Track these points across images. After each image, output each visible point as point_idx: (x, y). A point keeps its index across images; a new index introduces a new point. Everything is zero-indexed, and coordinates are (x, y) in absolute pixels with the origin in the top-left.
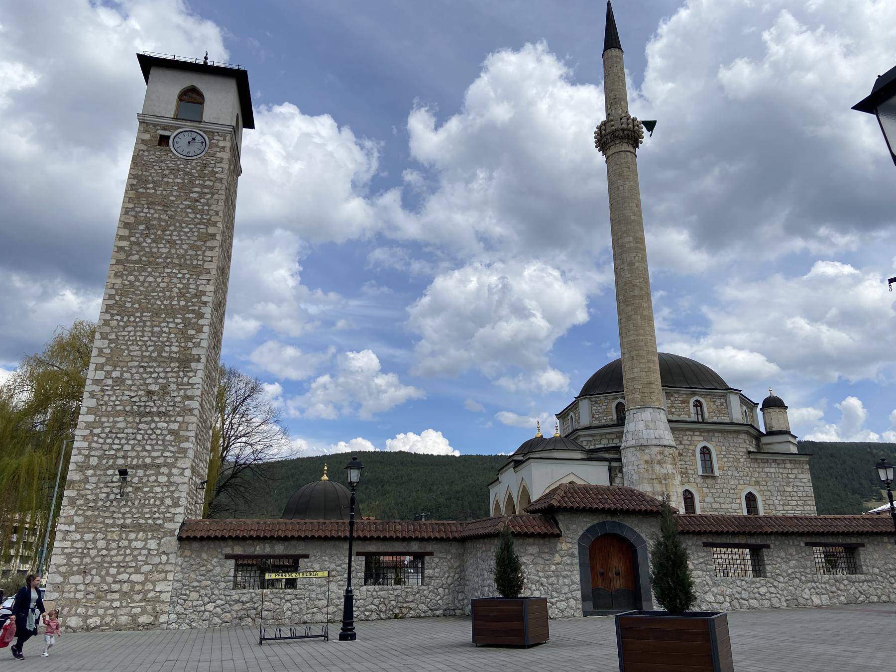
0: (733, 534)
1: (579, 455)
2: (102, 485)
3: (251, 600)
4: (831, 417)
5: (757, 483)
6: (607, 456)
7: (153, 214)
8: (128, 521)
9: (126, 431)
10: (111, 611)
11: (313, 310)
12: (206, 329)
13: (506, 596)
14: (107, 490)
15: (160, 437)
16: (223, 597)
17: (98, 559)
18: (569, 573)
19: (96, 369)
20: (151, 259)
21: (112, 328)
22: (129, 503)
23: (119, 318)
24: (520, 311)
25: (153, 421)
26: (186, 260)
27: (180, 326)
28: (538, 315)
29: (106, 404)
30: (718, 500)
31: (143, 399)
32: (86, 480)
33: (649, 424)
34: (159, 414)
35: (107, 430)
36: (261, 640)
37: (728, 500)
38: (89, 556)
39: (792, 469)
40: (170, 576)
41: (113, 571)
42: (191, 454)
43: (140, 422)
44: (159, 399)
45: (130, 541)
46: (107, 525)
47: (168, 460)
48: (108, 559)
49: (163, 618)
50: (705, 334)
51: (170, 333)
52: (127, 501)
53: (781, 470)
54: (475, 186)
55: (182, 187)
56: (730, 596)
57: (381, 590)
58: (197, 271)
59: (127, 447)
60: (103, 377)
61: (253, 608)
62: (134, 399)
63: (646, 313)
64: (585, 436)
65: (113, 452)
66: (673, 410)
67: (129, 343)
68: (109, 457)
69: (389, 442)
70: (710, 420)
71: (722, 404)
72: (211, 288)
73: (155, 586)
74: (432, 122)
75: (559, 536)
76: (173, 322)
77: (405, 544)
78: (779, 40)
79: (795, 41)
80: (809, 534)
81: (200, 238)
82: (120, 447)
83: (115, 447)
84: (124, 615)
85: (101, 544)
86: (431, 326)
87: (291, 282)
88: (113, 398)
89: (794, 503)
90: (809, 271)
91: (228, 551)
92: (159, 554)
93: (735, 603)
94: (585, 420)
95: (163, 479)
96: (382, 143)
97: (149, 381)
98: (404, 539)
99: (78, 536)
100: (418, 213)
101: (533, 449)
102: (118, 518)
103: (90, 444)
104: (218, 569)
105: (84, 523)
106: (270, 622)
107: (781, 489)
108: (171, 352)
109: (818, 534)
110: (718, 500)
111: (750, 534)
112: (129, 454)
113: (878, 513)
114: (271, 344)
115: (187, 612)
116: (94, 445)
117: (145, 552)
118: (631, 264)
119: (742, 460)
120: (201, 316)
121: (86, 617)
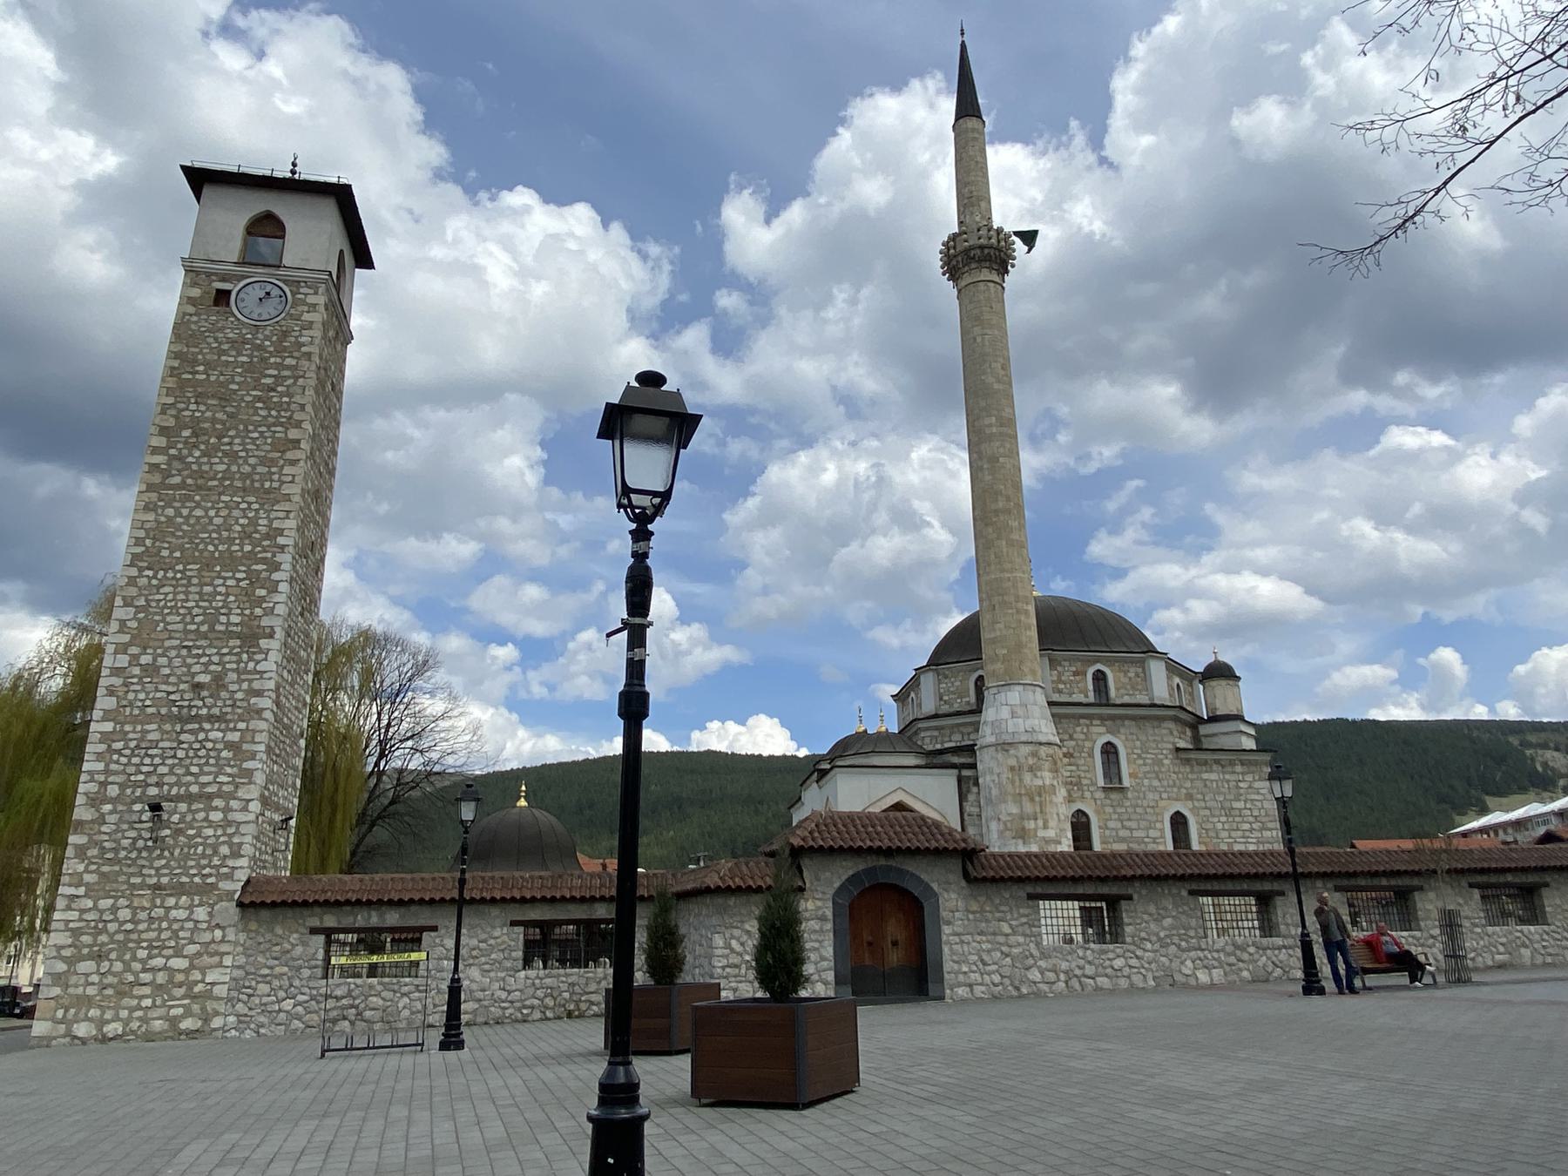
0: (1074, 880)
1: (911, 760)
3: (349, 994)
4: (1410, 679)
5: (1190, 797)
6: (956, 760)
8: (165, 880)
9: (161, 745)
10: (139, 1013)
11: (565, 521)
12: (283, 587)
13: (658, 982)
14: (133, 834)
16: (306, 990)
17: (120, 937)
18: (816, 945)
19: (116, 653)
20: (200, 482)
22: (166, 853)
23: (150, 573)
24: (907, 520)
25: (202, 729)
26: (253, 481)
28: (936, 524)
29: (131, 705)
30: (1127, 824)
31: (186, 696)
32: (101, 820)
33: (1019, 711)
34: (211, 718)
35: (133, 744)
36: (323, 1052)
37: (1143, 824)
38: (107, 931)
40: (228, 961)
41: (142, 954)
42: (260, 778)
43: (182, 731)
44: (211, 696)
47: (225, 788)
48: (134, 936)
49: (217, 1022)
50: (1210, 549)
51: (227, 595)
52: (162, 850)
54: (830, 313)
55: (249, 368)
56: (1066, 972)
57: (547, 976)
58: (270, 497)
59: (163, 770)
61: (352, 1006)
62: (172, 697)
63: (1015, 536)
64: (927, 729)
65: (141, 777)
66: (1061, 686)
68: (136, 785)
69: (696, 735)
70: (1118, 702)
71: (1137, 675)
72: (291, 523)
73: (204, 975)
74: (760, 211)
75: (802, 890)
76: (233, 578)
77: (585, 907)
78: (1328, 64)
79: (1353, 65)
80: (1340, 875)
81: (274, 447)
83: (145, 769)
85: (125, 914)
86: (763, 545)
87: (532, 479)
88: (142, 696)
89: (1246, 826)
90: (1378, 442)
91: (315, 922)
92: (211, 929)
93: (1075, 983)
94: (929, 705)
95: (216, 816)
96: (677, 250)
98: (583, 900)
99: (90, 904)
100: (740, 360)
101: (853, 750)
103: (107, 765)
104: (299, 949)
106: (377, 1027)
107: (1227, 805)
108: (229, 624)
109: (1208, 877)
110: (1127, 824)
111: (1103, 880)
112: (166, 779)
113: (1465, 835)
114: (500, 580)
115: (252, 1013)
116: (113, 767)
117: (190, 925)
118: (994, 459)
119: (1166, 762)
120: (277, 567)
121: (102, 1022)
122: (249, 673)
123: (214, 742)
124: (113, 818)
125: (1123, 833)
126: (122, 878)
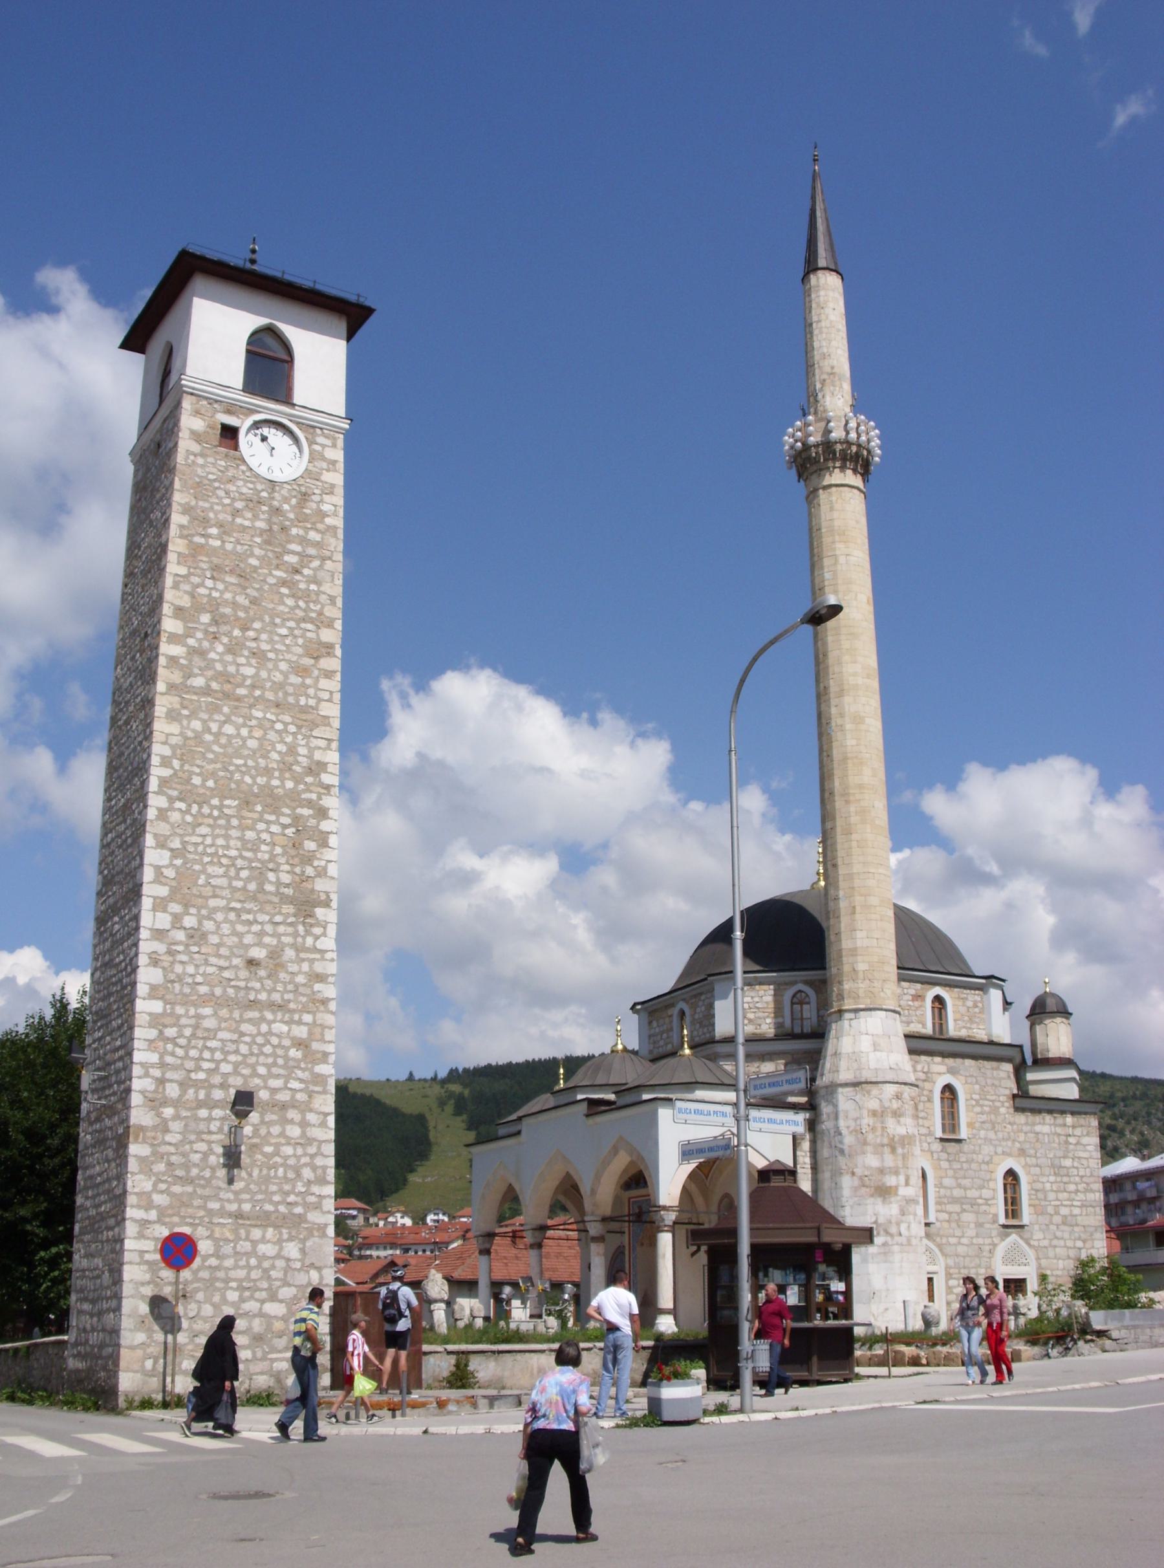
2: (193, 1137)
5: (1022, 1152)
7: (222, 593)
8: (247, 1207)
9: (221, 1035)
15: (280, 1052)
19: (154, 909)
21: (172, 825)
27: (290, 831)
34: (273, 1006)
35: (188, 1032)
39: (1074, 1127)
43: (242, 1021)
44: (269, 977)
45: (255, 1243)
46: (211, 1213)
53: (1059, 1130)
59: (226, 1068)
60: (168, 927)
62: (226, 974)
67: (207, 859)
68: (197, 1085)
76: (277, 822)
82: (213, 1066)
83: (206, 1065)
84: (262, 1373)
97: (248, 939)
102: (229, 1201)
105: (171, 1206)
107: (1057, 1162)
108: (279, 883)
117: (280, 1263)
120: (322, 813)
122: (308, 950)
123: (279, 1036)
124: (176, 1126)
125: (957, 1193)
126: (197, 1202)
